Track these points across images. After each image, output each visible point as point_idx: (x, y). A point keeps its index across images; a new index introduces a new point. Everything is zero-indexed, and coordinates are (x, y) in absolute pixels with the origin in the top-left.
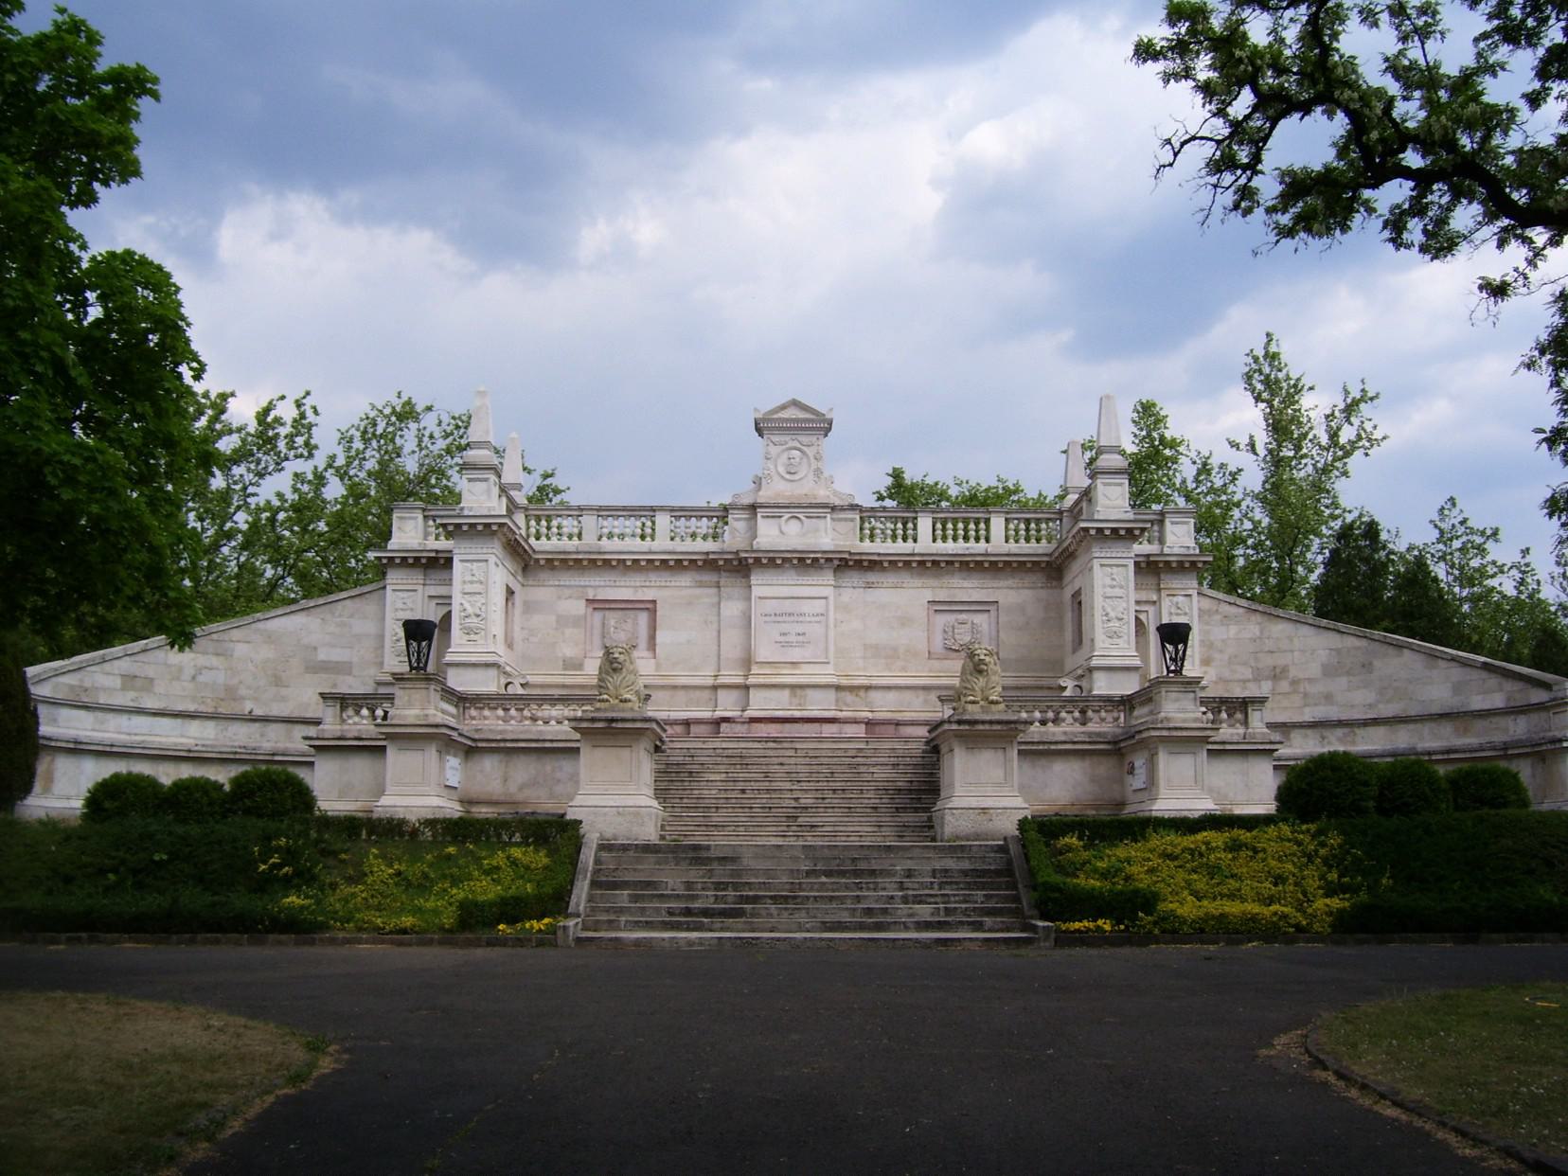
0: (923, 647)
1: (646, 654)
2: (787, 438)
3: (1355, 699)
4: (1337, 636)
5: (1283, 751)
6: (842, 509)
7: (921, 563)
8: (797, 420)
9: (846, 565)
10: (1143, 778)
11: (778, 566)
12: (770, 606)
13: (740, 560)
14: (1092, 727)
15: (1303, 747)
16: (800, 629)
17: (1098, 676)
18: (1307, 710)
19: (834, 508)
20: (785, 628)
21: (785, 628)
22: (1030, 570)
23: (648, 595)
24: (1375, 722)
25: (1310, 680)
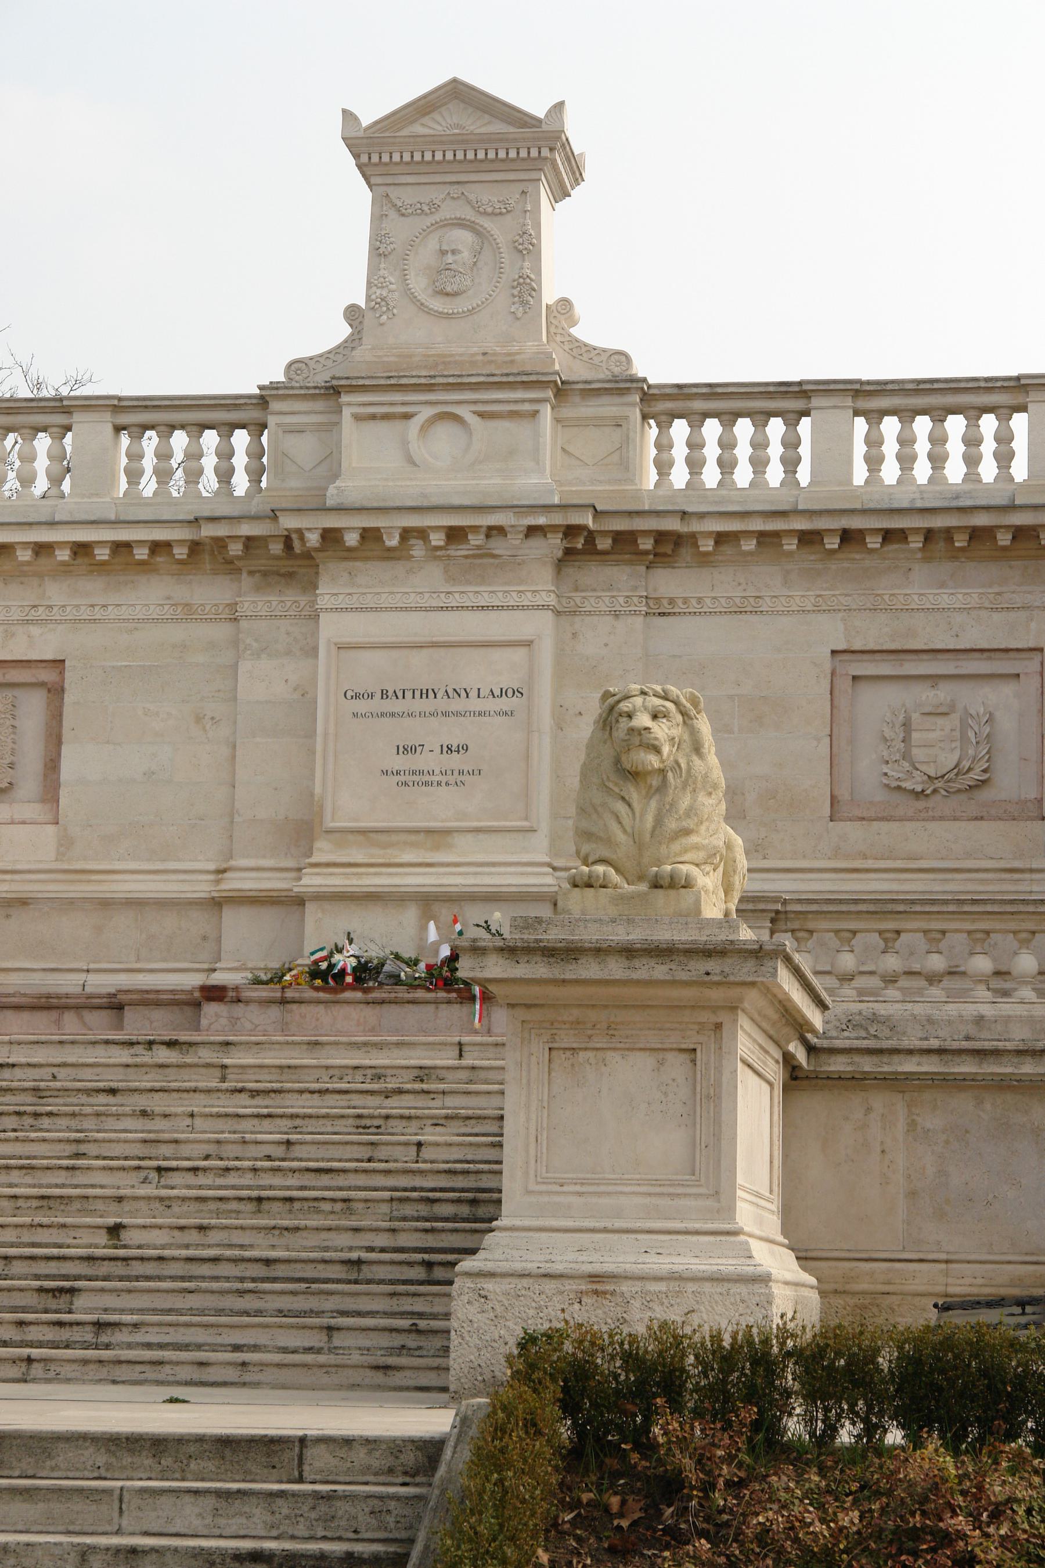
0: (816, 783)
1: (32, 811)
2: (436, 194)
6: (591, 392)
7: (809, 539)
8: (463, 141)
9: (590, 550)
11: (390, 555)
12: (370, 670)
16: (453, 732)
19: (562, 390)
20: (411, 731)
21: (411, 731)
23: (43, 644)
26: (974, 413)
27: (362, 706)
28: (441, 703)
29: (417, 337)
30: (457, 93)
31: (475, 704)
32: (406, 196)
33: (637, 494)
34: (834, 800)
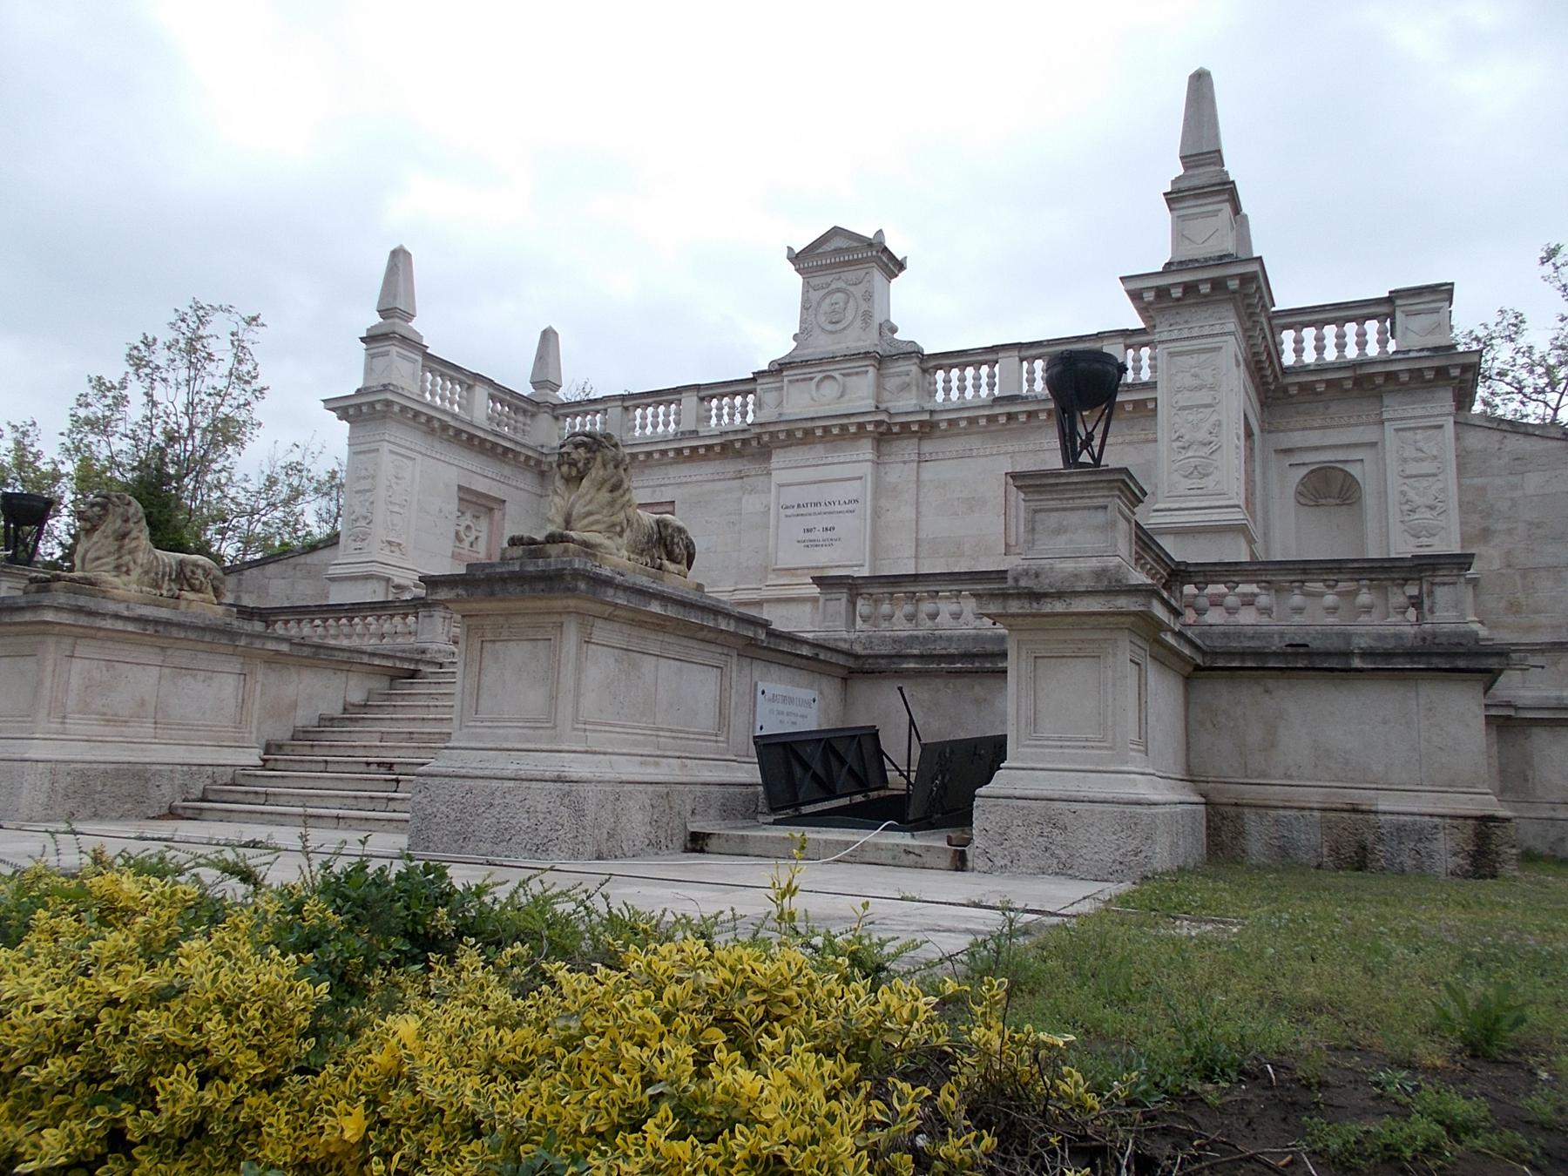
2: (829, 279)
12: (792, 496)
20: (811, 522)
21: (811, 522)
26: (1340, 322)
27: (789, 512)
28: (823, 508)
29: (824, 345)
30: (836, 232)
31: (837, 508)
32: (814, 281)
33: (634, 438)
34: (1006, 545)
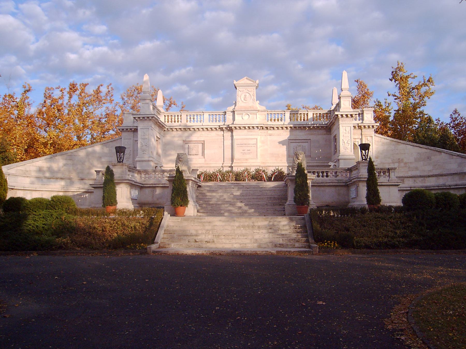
3: (427, 169)
4: (420, 149)
5: (402, 185)
10: (355, 194)
13: (230, 128)
14: (338, 178)
15: (409, 184)
16: (249, 148)
17: (230, 133)
18: (409, 172)
22: (320, 129)
24: (432, 176)
25: (411, 163)
